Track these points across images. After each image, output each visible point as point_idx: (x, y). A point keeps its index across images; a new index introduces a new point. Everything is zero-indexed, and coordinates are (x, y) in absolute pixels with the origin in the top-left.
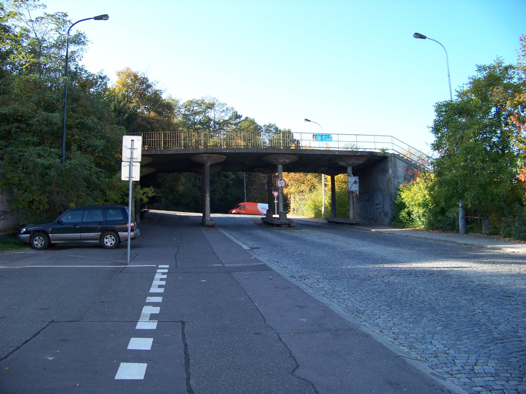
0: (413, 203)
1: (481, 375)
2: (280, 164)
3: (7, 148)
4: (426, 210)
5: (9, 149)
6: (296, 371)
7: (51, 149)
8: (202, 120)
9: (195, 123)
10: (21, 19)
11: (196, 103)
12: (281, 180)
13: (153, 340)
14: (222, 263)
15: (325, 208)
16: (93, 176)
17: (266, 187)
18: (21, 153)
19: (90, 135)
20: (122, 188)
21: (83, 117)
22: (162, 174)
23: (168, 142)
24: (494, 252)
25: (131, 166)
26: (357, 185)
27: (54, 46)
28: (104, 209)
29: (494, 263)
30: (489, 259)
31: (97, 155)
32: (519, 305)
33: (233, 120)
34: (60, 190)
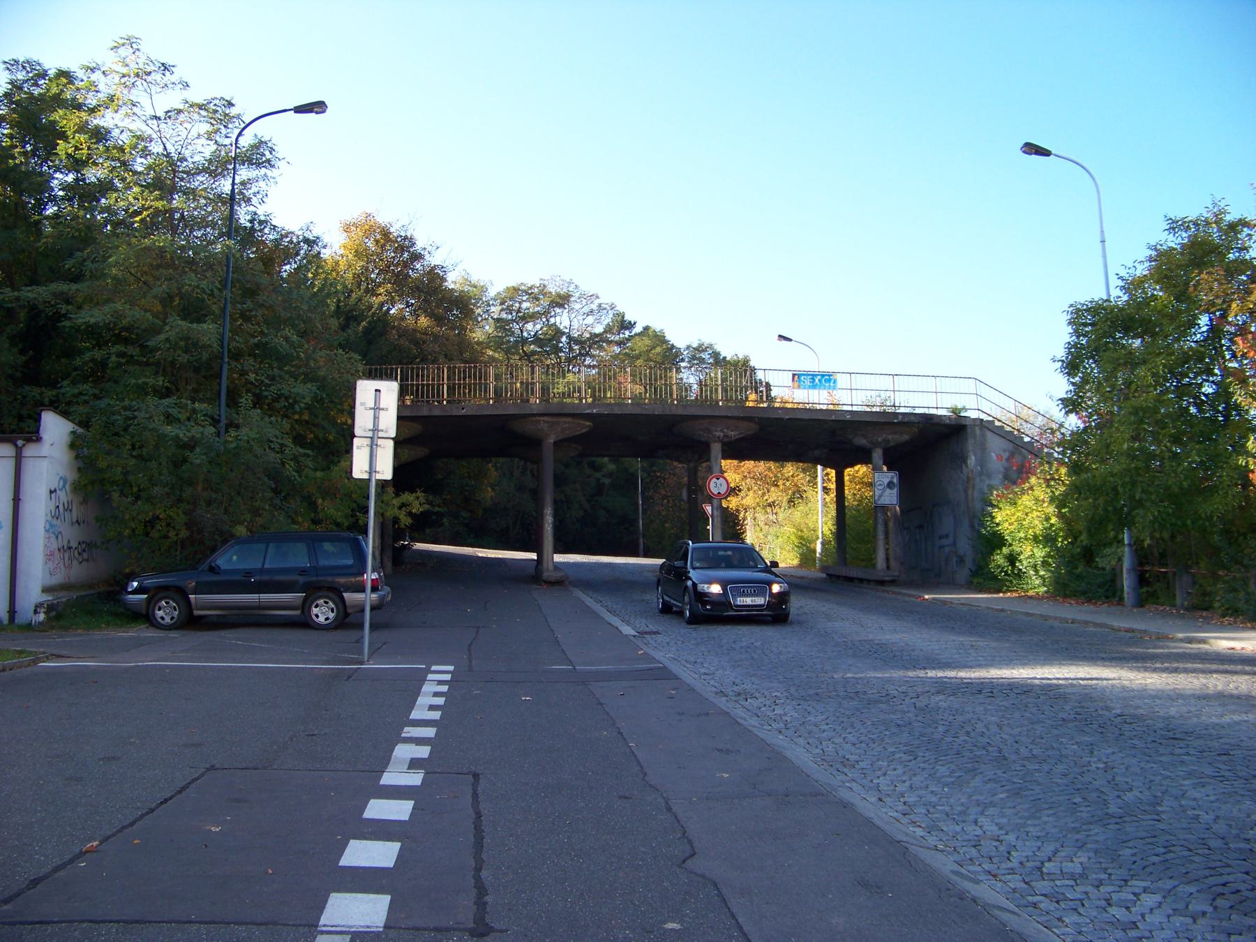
0: (1022, 535)
1: (1053, 877)
2: (716, 441)
3: (98, 402)
4: (1049, 552)
5: (102, 404)
6: (689, 862)
7: (194, 403)
8: (540, 332)
9: (524, 341)
10: (134, 113)
11: (527, 293)
12: (718, 479)
13: (414, 805)
14: (571, 663)
15: (823, 544)
16: (287, 466)
17: (685, 495)
18: (128, 413)
19: (282, 373)
20: (352, 493)
21: (266, 331)
22: (445, 460)
23: (459, 388)
24: (1192, 649)
25: (373, 447)
26: (895, 491)
27: (199, 172)
28: (313, 541)
29: (1176, 670)
30: (1167, 662)
31: (296, 417)
32: (1189, 755)
33: (613, 334)
34: (214, 496)
